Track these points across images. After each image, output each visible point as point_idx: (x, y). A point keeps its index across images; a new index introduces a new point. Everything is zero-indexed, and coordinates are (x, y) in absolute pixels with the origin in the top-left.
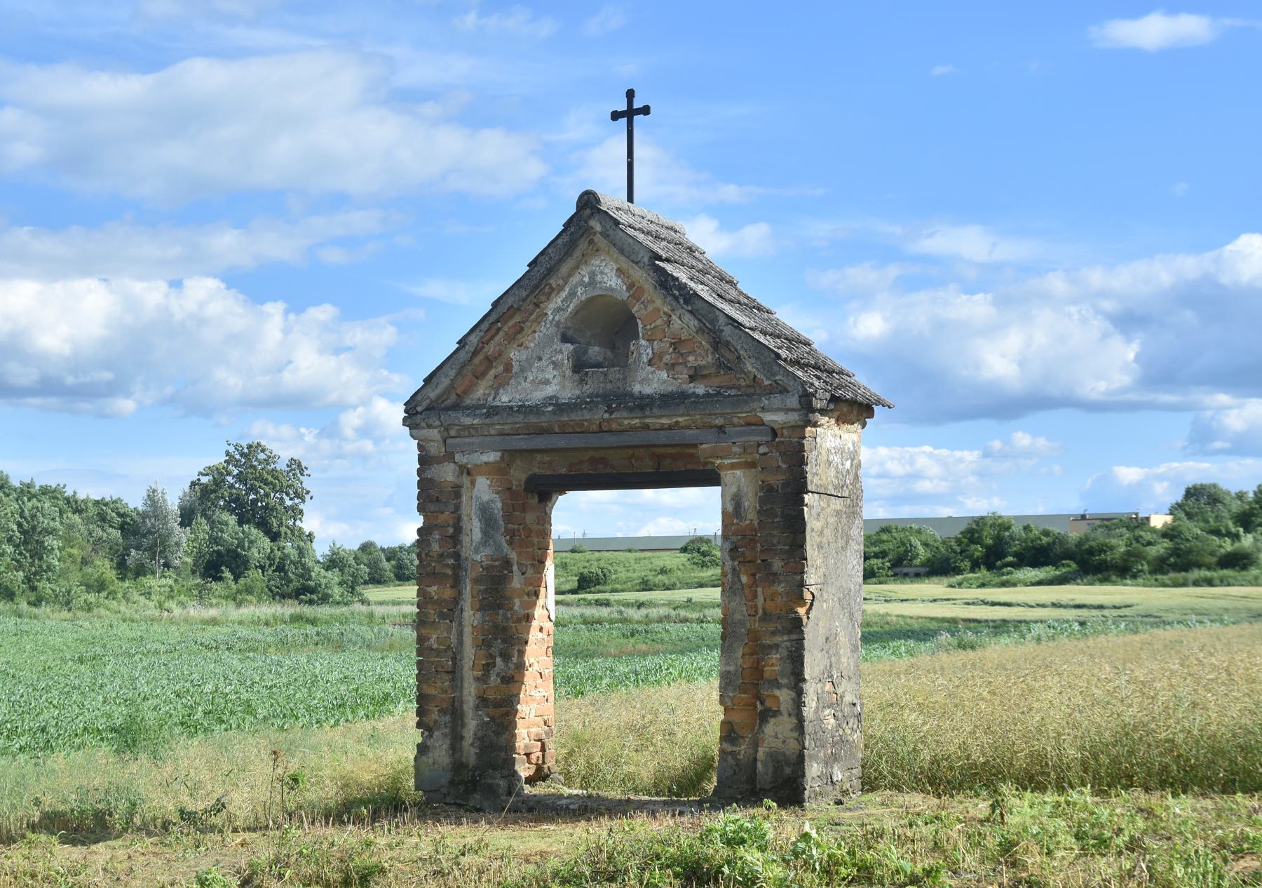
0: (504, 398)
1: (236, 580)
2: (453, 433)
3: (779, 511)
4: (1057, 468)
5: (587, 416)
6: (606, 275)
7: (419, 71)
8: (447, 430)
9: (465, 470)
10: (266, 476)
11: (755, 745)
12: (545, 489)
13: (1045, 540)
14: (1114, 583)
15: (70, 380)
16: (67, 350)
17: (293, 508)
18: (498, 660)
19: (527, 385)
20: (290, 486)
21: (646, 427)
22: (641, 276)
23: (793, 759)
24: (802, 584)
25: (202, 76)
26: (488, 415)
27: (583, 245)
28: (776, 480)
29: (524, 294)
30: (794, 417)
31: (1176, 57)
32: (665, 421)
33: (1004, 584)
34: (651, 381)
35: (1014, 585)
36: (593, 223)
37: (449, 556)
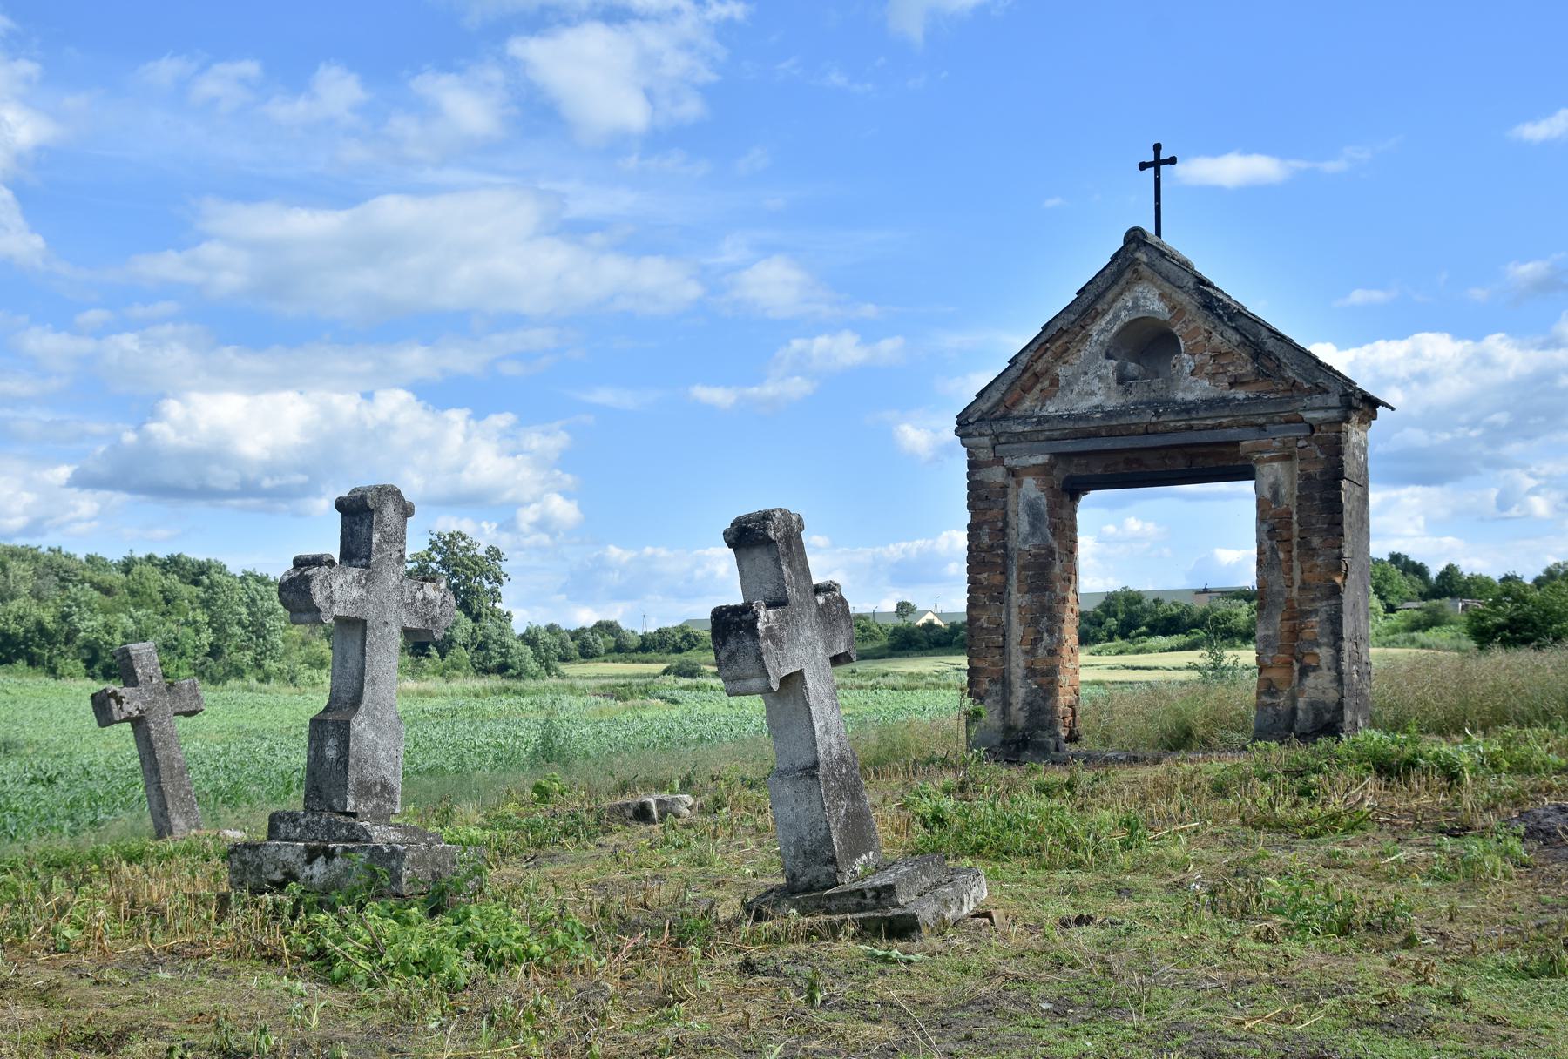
0: (1051, 409)
1: (442, 656)
3: (1317, 495)
4: (1166, 551)
5: (1135, 420)
6: (1150, 301)
7: (588, 202)
8: (997, 437)
9: (1012, 472)
12: (1073, 490)
13: (1176, 611)
14: (1239, 648)
16: (267, 456)
17: (493, 591)
19: (1074, 396)
21: (1190, 428)
24: (1340, 557)
25: (394, 211)
26: (1039, 423)
27: (1128, 275)
28: (1315, 470)
29: (1073, 318)
30: (1333, 414)
33: (1139, 651)
34: (1194, 389)
36: (1138, 255)
37: (999, 546)
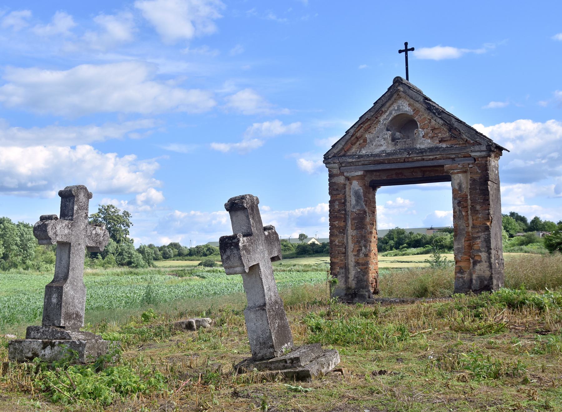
0: (364, 152)
1: (103, 258)
2: (343, 165)
3: (478, 188)
8: (341, 164)
9: (348, 178)
10: (114, 218)
11: (471, 275)
12: (374, 186)
13: (419, 237)
14: (447, 253)
15: (29, 185)
17: (125, 230)
18: (363, 248)
19: (373, 147)
20: (124, 221)
21: (423, 160)
22: (421, 107)
23: (488, 278)
24: (489, 214)
25: (86, 71)
26: (359, 158)
27: (395, 96)
29: (372, 114)
30: (483, 154)
31: (447, 63)
32: (431, 157)
33: (404, 255)
34: (424, 143)
35: (408, 255)
36: (399, 88)
